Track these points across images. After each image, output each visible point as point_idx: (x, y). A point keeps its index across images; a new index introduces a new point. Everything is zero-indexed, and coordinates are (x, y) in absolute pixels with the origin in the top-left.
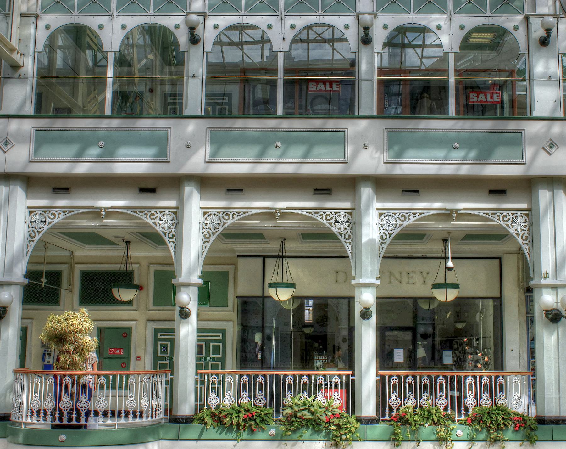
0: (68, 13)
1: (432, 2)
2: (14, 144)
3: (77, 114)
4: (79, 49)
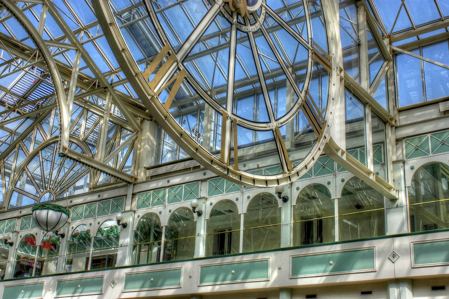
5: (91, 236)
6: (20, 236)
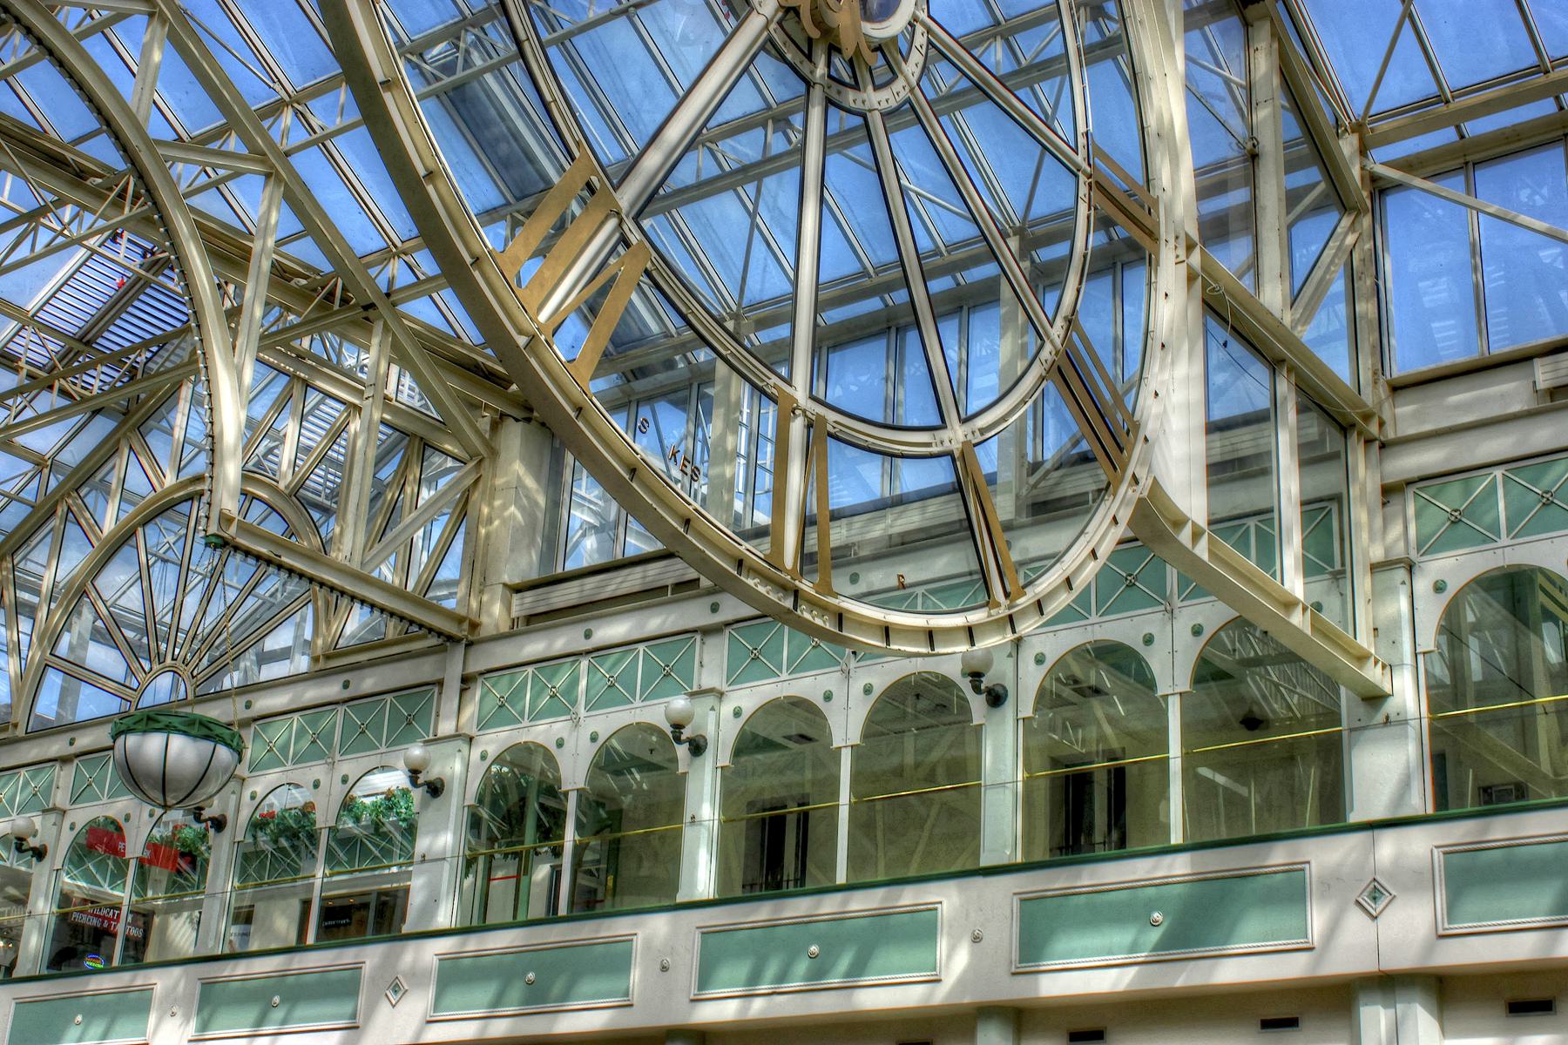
0: (1484, 542)
1: (1553, 502)
2: (1394, 893)
3: (1545, 798)
4: (1523, 627)
6: (68, 826)
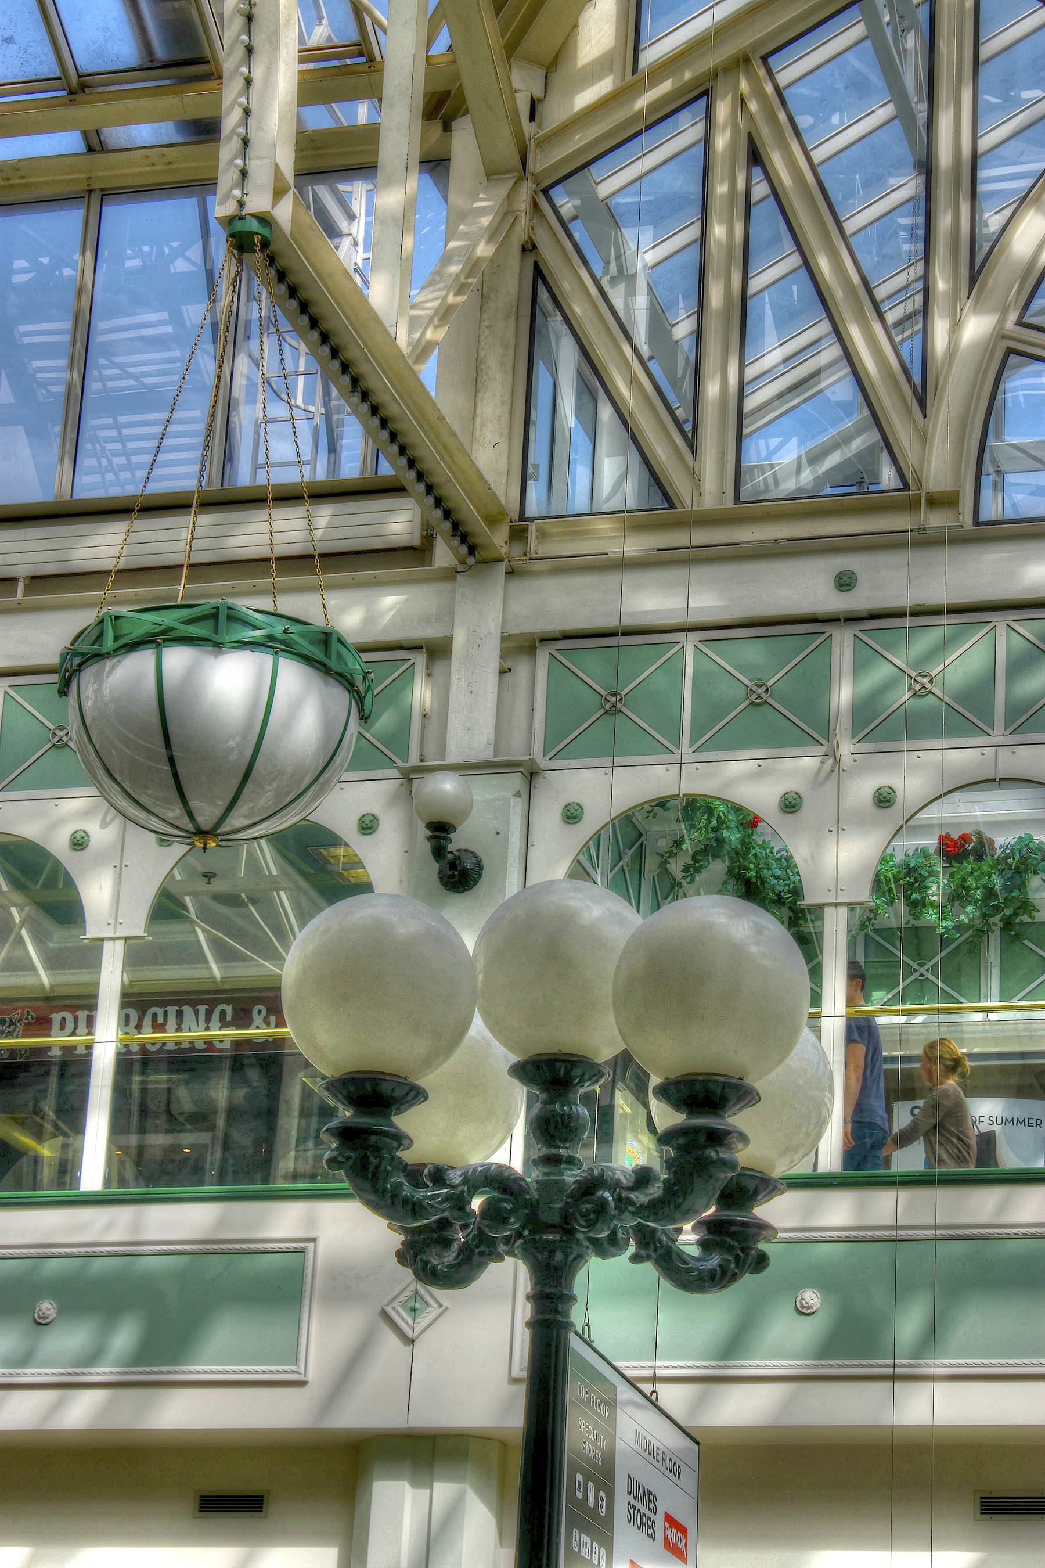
1: (766, 702)
5: (92, 931)
